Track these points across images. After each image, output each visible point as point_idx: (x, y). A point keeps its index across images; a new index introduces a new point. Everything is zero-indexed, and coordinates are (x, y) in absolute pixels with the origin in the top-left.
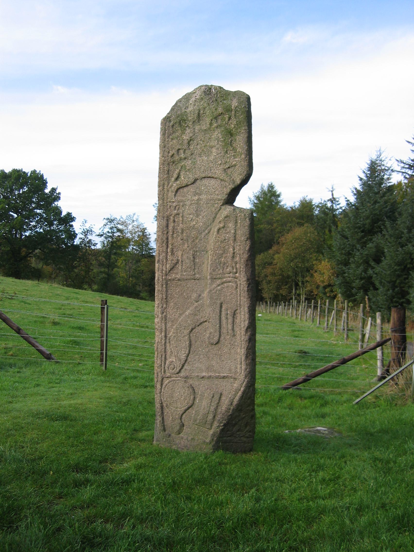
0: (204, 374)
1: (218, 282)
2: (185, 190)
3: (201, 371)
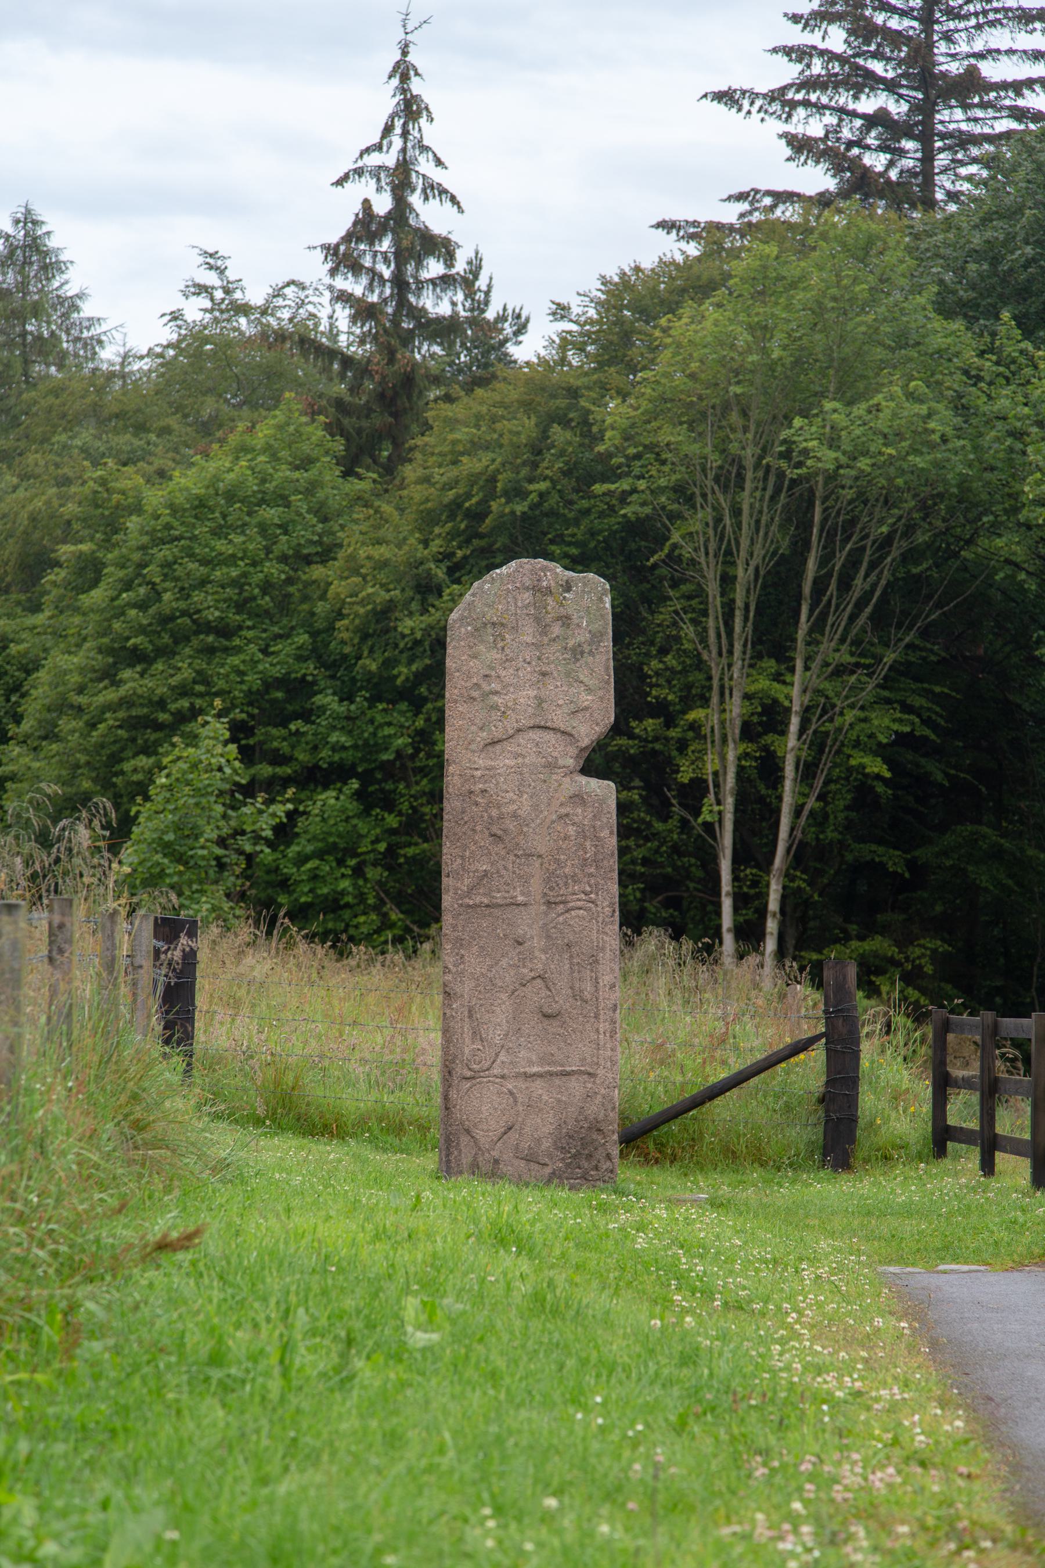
0: (535, 1069)
1: (561, 908)
2: (498, 747)
3: (531, 1063)
